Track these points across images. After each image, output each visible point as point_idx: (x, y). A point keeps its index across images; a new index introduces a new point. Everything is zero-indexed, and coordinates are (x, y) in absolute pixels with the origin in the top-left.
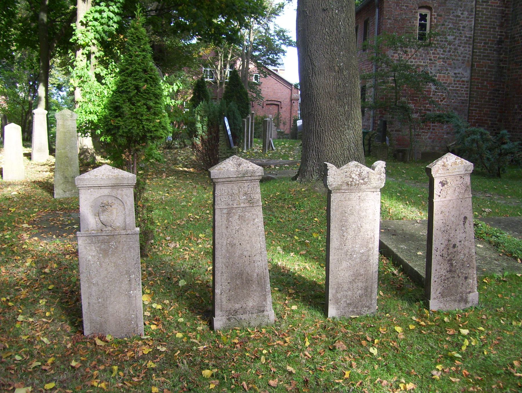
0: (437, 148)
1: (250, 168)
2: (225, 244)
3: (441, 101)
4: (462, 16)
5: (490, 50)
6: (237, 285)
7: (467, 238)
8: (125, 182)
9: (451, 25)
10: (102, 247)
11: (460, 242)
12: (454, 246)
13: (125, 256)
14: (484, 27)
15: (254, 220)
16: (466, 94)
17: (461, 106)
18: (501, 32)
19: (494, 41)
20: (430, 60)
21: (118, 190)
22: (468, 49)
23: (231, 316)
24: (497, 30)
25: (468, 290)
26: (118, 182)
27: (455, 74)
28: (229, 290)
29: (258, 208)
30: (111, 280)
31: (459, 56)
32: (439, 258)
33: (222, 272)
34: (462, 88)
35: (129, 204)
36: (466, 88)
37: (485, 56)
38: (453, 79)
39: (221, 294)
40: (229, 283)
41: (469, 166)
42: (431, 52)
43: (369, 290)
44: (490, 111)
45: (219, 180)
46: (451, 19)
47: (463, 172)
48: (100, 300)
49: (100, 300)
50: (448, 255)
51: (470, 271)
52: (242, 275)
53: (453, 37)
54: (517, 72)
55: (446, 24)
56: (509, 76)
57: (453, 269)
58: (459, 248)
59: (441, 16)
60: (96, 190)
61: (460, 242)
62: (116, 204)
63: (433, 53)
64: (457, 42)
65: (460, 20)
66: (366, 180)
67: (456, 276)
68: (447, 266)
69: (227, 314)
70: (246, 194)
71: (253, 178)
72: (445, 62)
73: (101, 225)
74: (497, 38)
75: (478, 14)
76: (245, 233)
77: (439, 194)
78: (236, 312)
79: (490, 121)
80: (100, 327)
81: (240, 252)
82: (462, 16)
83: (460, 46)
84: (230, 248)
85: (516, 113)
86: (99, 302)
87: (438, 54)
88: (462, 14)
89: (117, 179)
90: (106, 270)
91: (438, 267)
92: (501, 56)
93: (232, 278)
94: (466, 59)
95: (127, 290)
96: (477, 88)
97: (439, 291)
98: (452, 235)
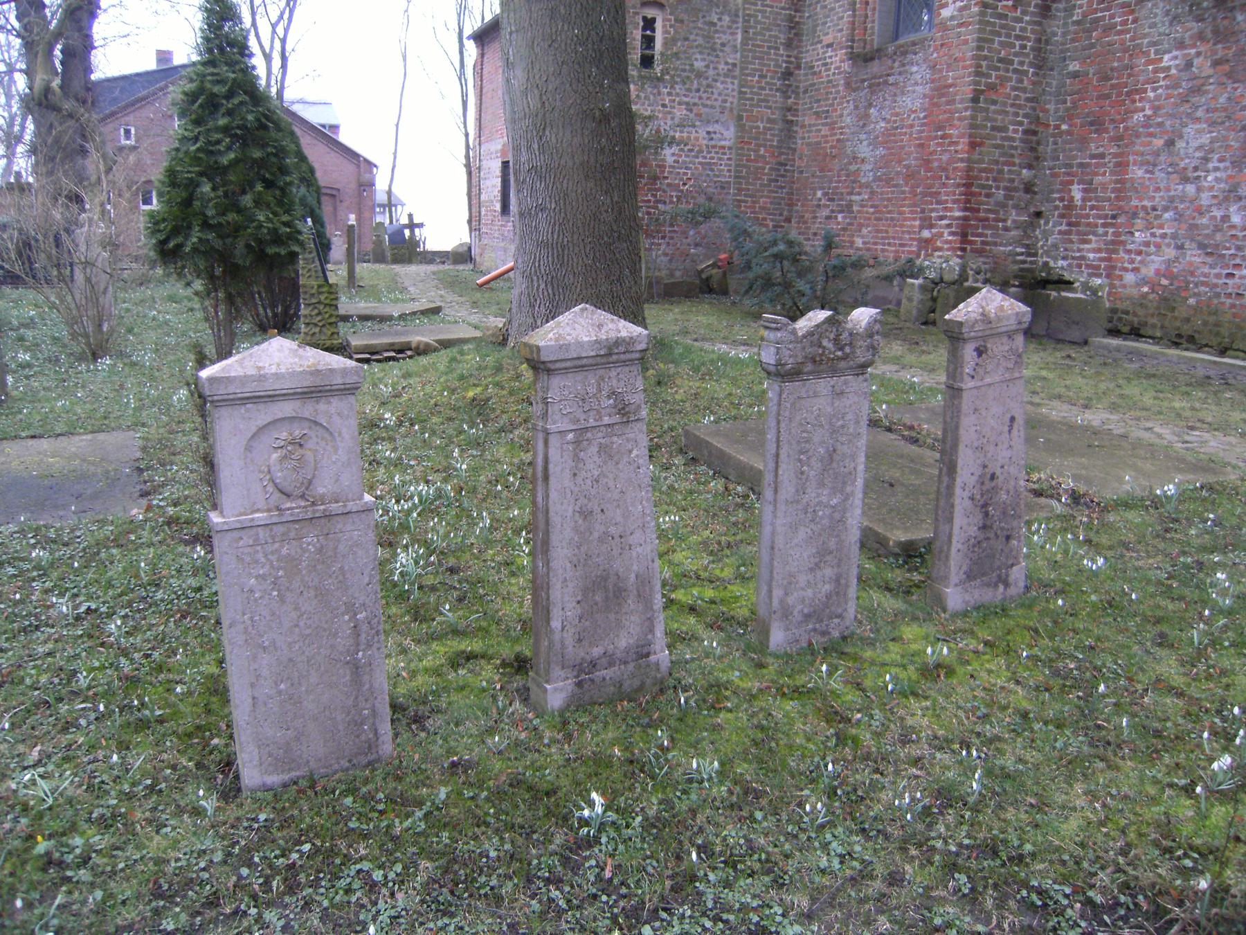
0: (678, 274)
1: (624, 334)
2: (570, 513)
3: (684, 184)
4: (719, 24)
5: (771, 90)
6: (596, 604)
7: (1014, 459)
8: (338, 380)
9: (700, 41)
10: (284, 551)
11: (1002, 467)
12: (993, 477)
13: (341, 568)
14: (759, 46)
15: (630, 452)
16: (729, 171)
17: (720, 194)
18: (789, 56)
19: (776, 72)
20: (664, 106)
21: (318, 402)
22: (730, 86)
23: (583, 676)
24: (781, 52)
25: (1010, 563)
26: (318, 381)
27: (708, 133)
28: (580, 618)
29: (639, 425)
30: (308, 631)
31: (716, 100)
32: (968, 503)
33: (565, 580)
34: (720, 159)
35: (347, 437)
36: (729, 159)
37: (763, 101)
38: (705, 142)
39: (563, 629)
40: (579, 602)
41: (1024, 314)
42: (665, 91)
43: (843, 582)
44: (771, 203)
45: (558, 365)
46: (700, 29)
47: (1014, 327)
48: (282, 686)
49: (282, 686)
50: (982, 495)
51: (1015, 524)
52: (606, 580)
53: (703, 64)
54: (820, 131)
55: (692, 37)
56: (803, 138)
57: (988, 523)
58: (1001, 478)
59: (682, 21)
60: (261, 406)
61: (1002, 467)
62: (315, 439)
63: (669, 94)
64: (711, 73)
65: (716, 32)
66: (847, 350)
67: (992, 535)
68: (978, 518)
69: (575, 673)
70: (613, 393)
71: (628, 356)
72: (691, 111)
73: (277, 495)
74: (781, 67)
75: (748, 21)
76: (611, 484)
77: (972, 373)
78: (594, 665)
79: (772, 220)
80: (286, 752)
81: (603, 528)
82: (719, 24)
83: (716, 81)
84: (580, 521)
85: (819, 206)
86: (280, 693)
87: (678, 95)
88: (720, 19)
89: (316, 373)
90: (295, 609)
91: (965, 521)
92: (790, 101)
93: (586, 591)
94: (728, 105)
95: (348, 651)
96: (748, 160)
97: (965, 568)
98: (989, 455)
